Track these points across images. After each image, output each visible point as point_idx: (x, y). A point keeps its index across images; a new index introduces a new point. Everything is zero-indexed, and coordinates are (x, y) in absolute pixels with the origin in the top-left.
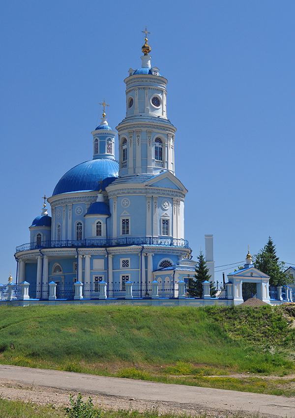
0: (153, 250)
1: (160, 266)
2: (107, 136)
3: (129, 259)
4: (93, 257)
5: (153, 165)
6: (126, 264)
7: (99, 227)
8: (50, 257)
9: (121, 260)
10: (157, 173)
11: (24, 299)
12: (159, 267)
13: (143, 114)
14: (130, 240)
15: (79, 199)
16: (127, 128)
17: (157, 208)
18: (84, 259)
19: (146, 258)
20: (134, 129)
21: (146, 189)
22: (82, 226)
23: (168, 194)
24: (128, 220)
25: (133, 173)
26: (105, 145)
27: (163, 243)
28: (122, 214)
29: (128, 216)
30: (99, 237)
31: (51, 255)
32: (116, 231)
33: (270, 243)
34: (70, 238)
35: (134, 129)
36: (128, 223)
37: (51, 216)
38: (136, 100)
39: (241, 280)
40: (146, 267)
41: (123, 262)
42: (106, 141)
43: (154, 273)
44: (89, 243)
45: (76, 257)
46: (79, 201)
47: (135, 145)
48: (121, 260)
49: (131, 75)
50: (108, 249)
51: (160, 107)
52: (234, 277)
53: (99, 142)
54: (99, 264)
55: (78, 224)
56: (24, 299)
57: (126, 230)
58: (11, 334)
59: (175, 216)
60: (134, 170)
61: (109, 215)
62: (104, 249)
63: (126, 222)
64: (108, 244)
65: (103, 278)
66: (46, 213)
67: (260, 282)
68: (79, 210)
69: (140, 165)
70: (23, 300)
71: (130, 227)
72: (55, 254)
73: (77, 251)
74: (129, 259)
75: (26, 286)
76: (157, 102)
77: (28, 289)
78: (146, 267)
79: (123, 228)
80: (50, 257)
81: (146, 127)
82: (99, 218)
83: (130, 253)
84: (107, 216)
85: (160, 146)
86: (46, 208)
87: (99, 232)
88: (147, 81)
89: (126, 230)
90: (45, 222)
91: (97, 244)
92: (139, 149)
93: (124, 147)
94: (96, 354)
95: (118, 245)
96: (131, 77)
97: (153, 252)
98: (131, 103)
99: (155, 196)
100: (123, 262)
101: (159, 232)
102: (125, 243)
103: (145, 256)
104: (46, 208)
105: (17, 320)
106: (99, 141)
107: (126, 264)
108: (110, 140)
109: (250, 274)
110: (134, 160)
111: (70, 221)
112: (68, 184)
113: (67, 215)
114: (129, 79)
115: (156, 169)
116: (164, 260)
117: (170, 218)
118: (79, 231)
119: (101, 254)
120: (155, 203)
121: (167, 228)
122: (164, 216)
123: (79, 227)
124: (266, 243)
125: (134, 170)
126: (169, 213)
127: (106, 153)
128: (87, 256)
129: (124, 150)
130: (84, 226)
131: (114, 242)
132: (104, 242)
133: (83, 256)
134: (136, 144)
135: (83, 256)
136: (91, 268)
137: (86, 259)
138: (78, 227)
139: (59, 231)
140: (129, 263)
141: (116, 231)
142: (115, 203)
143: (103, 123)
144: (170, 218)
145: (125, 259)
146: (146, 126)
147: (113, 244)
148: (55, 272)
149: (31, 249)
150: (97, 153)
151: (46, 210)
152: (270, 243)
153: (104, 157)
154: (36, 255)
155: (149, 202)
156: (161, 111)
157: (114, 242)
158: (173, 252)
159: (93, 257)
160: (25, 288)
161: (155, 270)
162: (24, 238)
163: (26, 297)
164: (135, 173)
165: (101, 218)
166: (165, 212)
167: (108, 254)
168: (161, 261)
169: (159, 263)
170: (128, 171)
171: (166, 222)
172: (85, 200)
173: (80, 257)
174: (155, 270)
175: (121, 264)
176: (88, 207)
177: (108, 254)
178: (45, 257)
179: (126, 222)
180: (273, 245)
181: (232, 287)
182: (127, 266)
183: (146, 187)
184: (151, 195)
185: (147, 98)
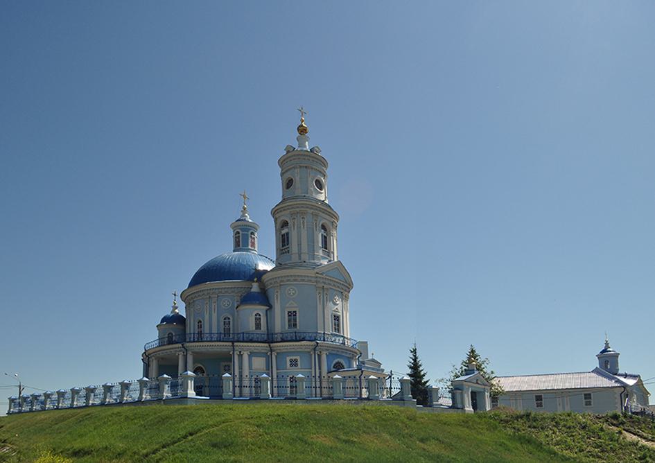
0: (327, 348)
1: (334, 367)
2: (250, 229)
3: (298, 358)
4: (251, 355)
5: (320, 253)
7: (258, 320)
8: (195, 354)
9: (288, 359)
10: (325, 262)
11: (189, 396)
14: (299, 334)
15: (226, 290)
16: (288, 209)
17: (328, 302)
18: (241, 356)
20: (298, 210)
22: (231, 320)
24: (295, 312)
25: (297, 258)
26: (248, 239)
27: (337, 341)
28: (288, 305)
29: (296, 307)
30: (258, 331)
31: (197, 350)
32: (280, 324)
34: (215, 330)
35: (298, 210)
36: (295, 315)
37: (185, 317)
38: (297, 179)
39: (469, 386)
40: (320, 368)
41: (291, 361)
42: (249, 233)
43: (329, 375)
45: (231, 353)
46: (226, 292)
47: (299, 227)
48: (288, 359)
49: (288, 152)
50: (272, 345)
51: (323, 191)
52: (465, 383)
53: (240, 235)
54: (259, 363)
55: (225, 319)
56: (189, 396)
58: (214, 445)
59: (344, 313)
60: (300, 256)
61: (270, 307)
62: (267, 345)
63: (292, 315)
64: (270, 339)
66: (177, 311)
67: (483, 390)
68: (226, 303)
69: (306, 251)
70: (186, 397)
71: (298, 320)
72: (203, 350)
73: (233, 346)
74: (298, 358)
75: (190, 377)
76: (320, 185)
77: (193, 382)
78: (320, 368)
80: (195, 354)
81: (312, 208)
82: (257, 309)
83: (300, 350)
84: (268, 308)
86: (176, 305)
87: (258, 326)
90: (175, 320)
91: (258, 338)
92: (304, 234)
93: (284, 232)
95: (283, 341)
96: (289, 154)
97: (327, 350)
98: (289, 184)
100: (291, 361)
101: (331, 329)
102: (294, 338)
103: (239, 355)
104: (176, 305)
105: (210, 423)
106: (241, 233)
107: (294, 363)
108: (252, 233)
109: (475, 381)
110: (299, 245)
111: (215, 315)
112: (207, 274)
113: (210, 308)
114: (285, 157)
115: (324, 258)
117: (341, 314)
118: (227, 326)
119: (263, 351)
121: (338, 325)
122: (334, 311)
125: (300, 256)
126: (339, 307)
127: (250, 247)
128: (245, 353)
129: (283, 236)
130: (233, 320)
133: (240, 352)
134: (300, 227)
135: (240, 352)
136: (250, 367)
137: (244, 356)
138: (224, 322)
140: (299, 363)
141: (280, 324)
142: (277, 292)
143: (243, 215)
144: (341, 314)
145: (294, 358)
146: (312, 207)
147: (278, 340)
149: (159, 346)
150: (239, 246)
151: (176, 308)
153: (248, 250)
154: (176, 351)
155: (319, 293)
156: (323, 195)
158: (343, 352)
159: (251, 355)
160: (189, 381)
162: (151, 336)
163: (191, 393)
164: (300, 259)
165: (261, 309)
166: (336, 307)
167: (271, 351)
168: (334, 362)
169: (333, 365)
170: (291, 257)
171: (337, 318)
172: (232, 292)
173: (237, 353)
174: (329, 372)
175: (288, 363)
176: (239, 299)
177: (271, 351)
178: (189, 353)
179: (292, 315)
181: (462, 394)
184: (321, 285)
185: (310, 179)
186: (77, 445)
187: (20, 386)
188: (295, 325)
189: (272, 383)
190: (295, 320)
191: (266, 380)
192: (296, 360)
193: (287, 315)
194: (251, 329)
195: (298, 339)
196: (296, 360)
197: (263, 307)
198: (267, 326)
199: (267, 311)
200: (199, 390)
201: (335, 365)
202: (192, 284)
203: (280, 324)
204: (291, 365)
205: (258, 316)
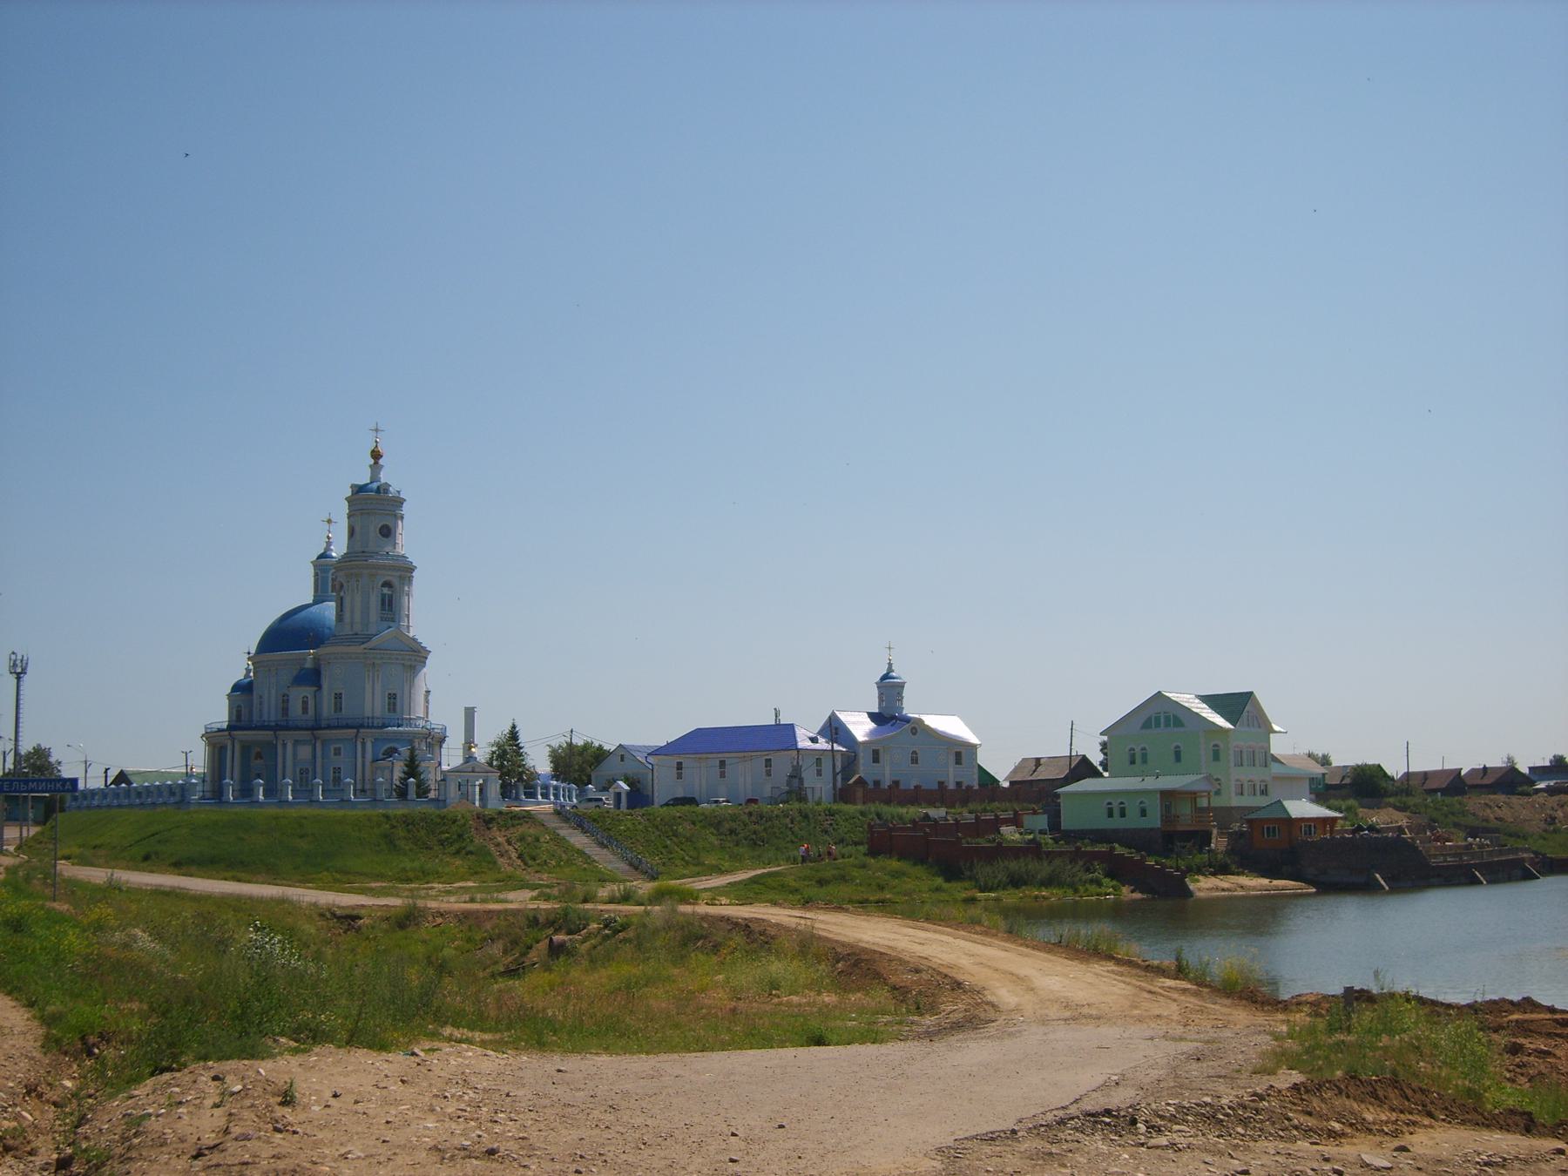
1: (384, 754)
3: (341, 746)
4: (296, 743)
6: (337, 752)
7: (305, 703)
12: (381, 756)
13: (366, 550)
18: (284, 745)
19: (364, 744)
21: (365, 653)
23: (397, 659)
24: (341, 694)
33: (514, 727)
35: (353, 571)
40: (363, 757)
45: (274, 742)
50: (315, 732)
57: (338, 708)
61: (320, 687)
62: (309, 732)
63: (338, 696)
65: (310, 769)
74: (341, 746)
79: (336, 704)
84: (316, 688)
85: (390, 593)
87: (305, 710)
88: (372, 503)
89: (338, 708)
94: (242, 862)
95: (329, 727)
99: (377, 662)
100: (335, 749)
110: (352, 612)
111: (273, 692)
116: (392, 745)
120: (378, 671)
121: (395, 704)
123: (285, 699)
124: (507, 729)
131: (324, 724)
132: (310, 724)
139: (261, 703)
145: (337, 746)
148: (256, 759)
152: (514, 727)
157: (324, 724)
159: (296, 743)
161: (375, 760)
165: (308, 691)
168: (385, 748)
169: (382, 751)
175: (332, 752)
176: (295, 673)
178: (236, 741)
179: (338, 696)
180: (517, 729)
182: (340, 754)
183: (366, 651)
186: (98, 842)
187: (86, 762)
188: (287, 715)
189: (355, 787)
190: (341, 704)
191: (349, 784)
192: (340, 749)
193: (333, 698)
194: (368, 713)
195: (375, 725)
196: (340, 749)
197: (308, 688)
198: (315, 710)
199: (315, 692)
200: (500, 991)
201: (386, 751)
202: (318, 558)
203: (327, 709)
204: (335, 754)
205: (305, 699)
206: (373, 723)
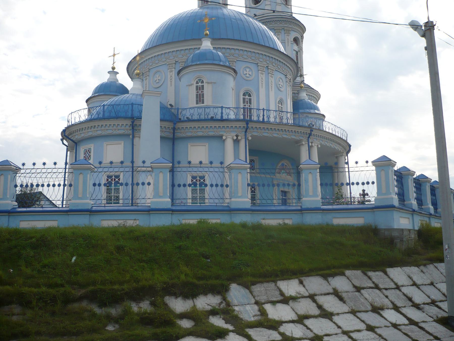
44: (199, 114)
140: (92, 154)
206: (269, 117)
